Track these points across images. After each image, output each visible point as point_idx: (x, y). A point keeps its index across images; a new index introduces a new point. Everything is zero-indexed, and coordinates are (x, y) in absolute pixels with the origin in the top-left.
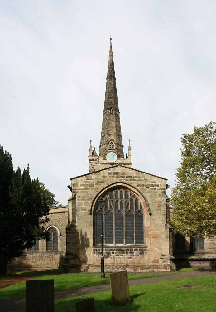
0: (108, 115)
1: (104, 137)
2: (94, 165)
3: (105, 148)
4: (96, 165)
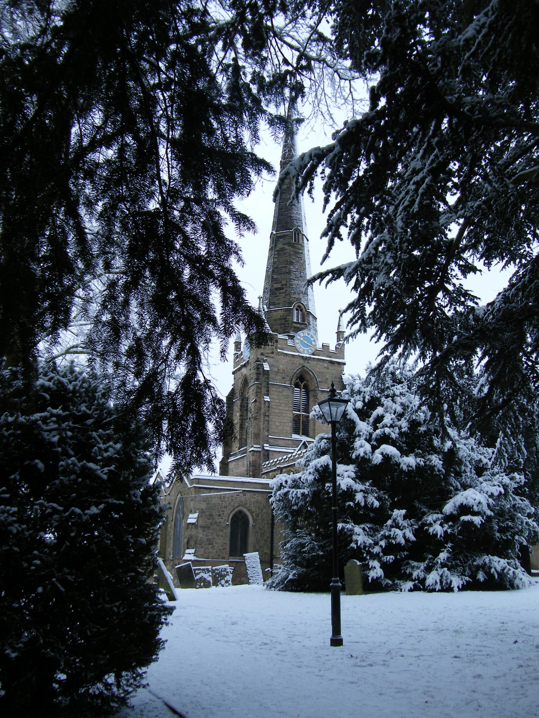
0: (289, 244)
1: (282, 291)
2: (267, 356)
3: (285, 319)
4: (272, 355)
